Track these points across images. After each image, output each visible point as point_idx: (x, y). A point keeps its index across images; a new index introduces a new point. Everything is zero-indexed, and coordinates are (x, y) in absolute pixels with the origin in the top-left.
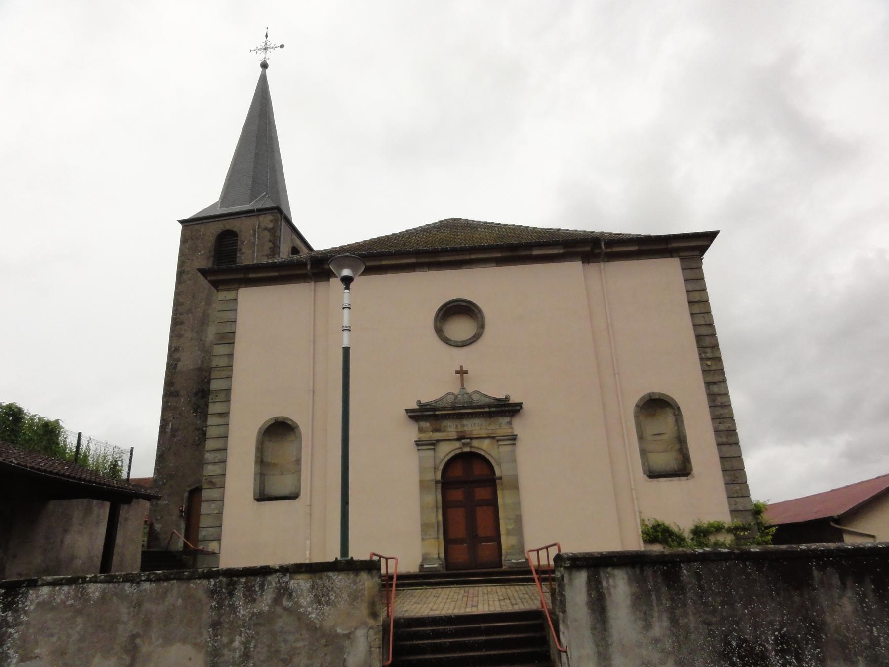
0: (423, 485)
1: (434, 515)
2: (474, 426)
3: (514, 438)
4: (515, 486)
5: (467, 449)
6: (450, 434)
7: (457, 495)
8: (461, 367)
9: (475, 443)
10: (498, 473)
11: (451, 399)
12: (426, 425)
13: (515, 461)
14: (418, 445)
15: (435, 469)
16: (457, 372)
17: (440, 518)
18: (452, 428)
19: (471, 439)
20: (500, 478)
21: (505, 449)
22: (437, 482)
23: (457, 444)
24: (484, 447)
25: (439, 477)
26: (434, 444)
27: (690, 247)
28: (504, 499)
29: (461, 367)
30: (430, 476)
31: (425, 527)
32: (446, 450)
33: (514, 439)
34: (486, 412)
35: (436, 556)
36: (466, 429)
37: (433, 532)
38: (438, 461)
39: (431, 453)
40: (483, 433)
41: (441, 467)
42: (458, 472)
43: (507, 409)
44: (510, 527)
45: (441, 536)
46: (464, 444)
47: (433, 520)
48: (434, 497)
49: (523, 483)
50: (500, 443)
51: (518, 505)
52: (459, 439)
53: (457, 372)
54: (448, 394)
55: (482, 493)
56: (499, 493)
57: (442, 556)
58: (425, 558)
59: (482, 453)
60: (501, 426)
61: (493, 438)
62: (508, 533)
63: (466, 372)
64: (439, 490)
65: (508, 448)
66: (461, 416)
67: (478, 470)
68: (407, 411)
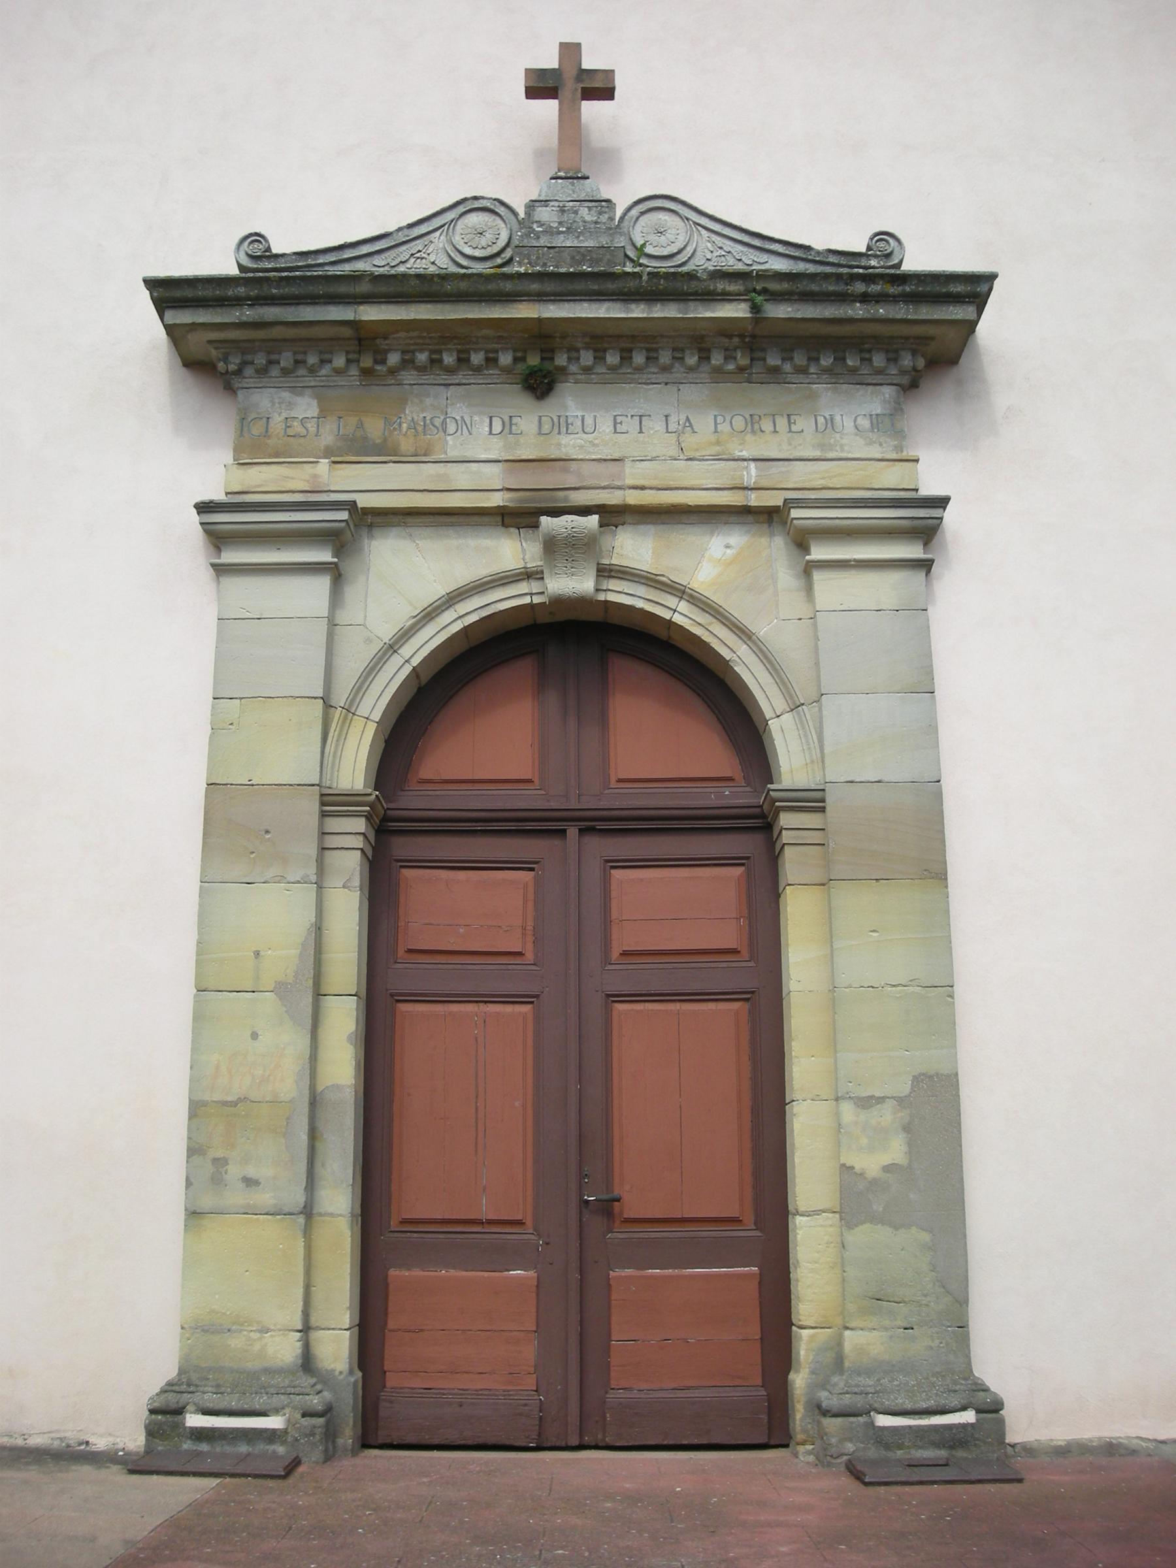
0: (232, 821)
1: (294, 1042)
2: (633, 437)
3: (919, 523)
4: (914, 849)
5: (574, 583)
6: (461, 477)
7: (475, 905)
8: (570, 51)
9: (633, 548)
10: (792, 765)
11: (479, 239)
12: (295, 409)
13: (924, 686)
14: (217, 538)
15: (331, 710)
16: (541, 86)
17: (341, 1067)
18: (476, 442)
19: (613, 516)
20: (813, 801)
21: (854, 596)
22: (332, 803)
23: (509, 551)
24: (705, 578)
25: (354, 770)
26: (345, 533)
27: (667, 432)
28: (825, 949)
29: (570, 51)
30: (288, 756)
31: (213, 1121)
32: (419, 591)
33: (927, 533)
34: (726, 328)
35: (286, 1350)
36: (569, 445)
37: (272, 1166)
38: (354, 658)
39: (313, 593)
40: (703, 483)
41: (378, 701)
42: (500, 745)
43: (892, 327)
44: (870, 1163)
45: (339, 1200)
46: (552, 546)
47: (287, 1084)
48: (315, 911)
49: (973, 843)
50: (819, 552)
51: (934, 1000)
52: (518, 517)
53: (541, 86)
54: (469, 205)
55: (668, 903)
56: (799, 910)
57: (336, 1349)
58: (202, 1329)
59: (683, 615)
60: (828, 441)
61: (768, 517)
62: (855, 1201)
63: (600, 88)
64: (349, 864)
65: (885, 588)
66: (538, 367)
67: (650, 743)
68: (168, 294)
